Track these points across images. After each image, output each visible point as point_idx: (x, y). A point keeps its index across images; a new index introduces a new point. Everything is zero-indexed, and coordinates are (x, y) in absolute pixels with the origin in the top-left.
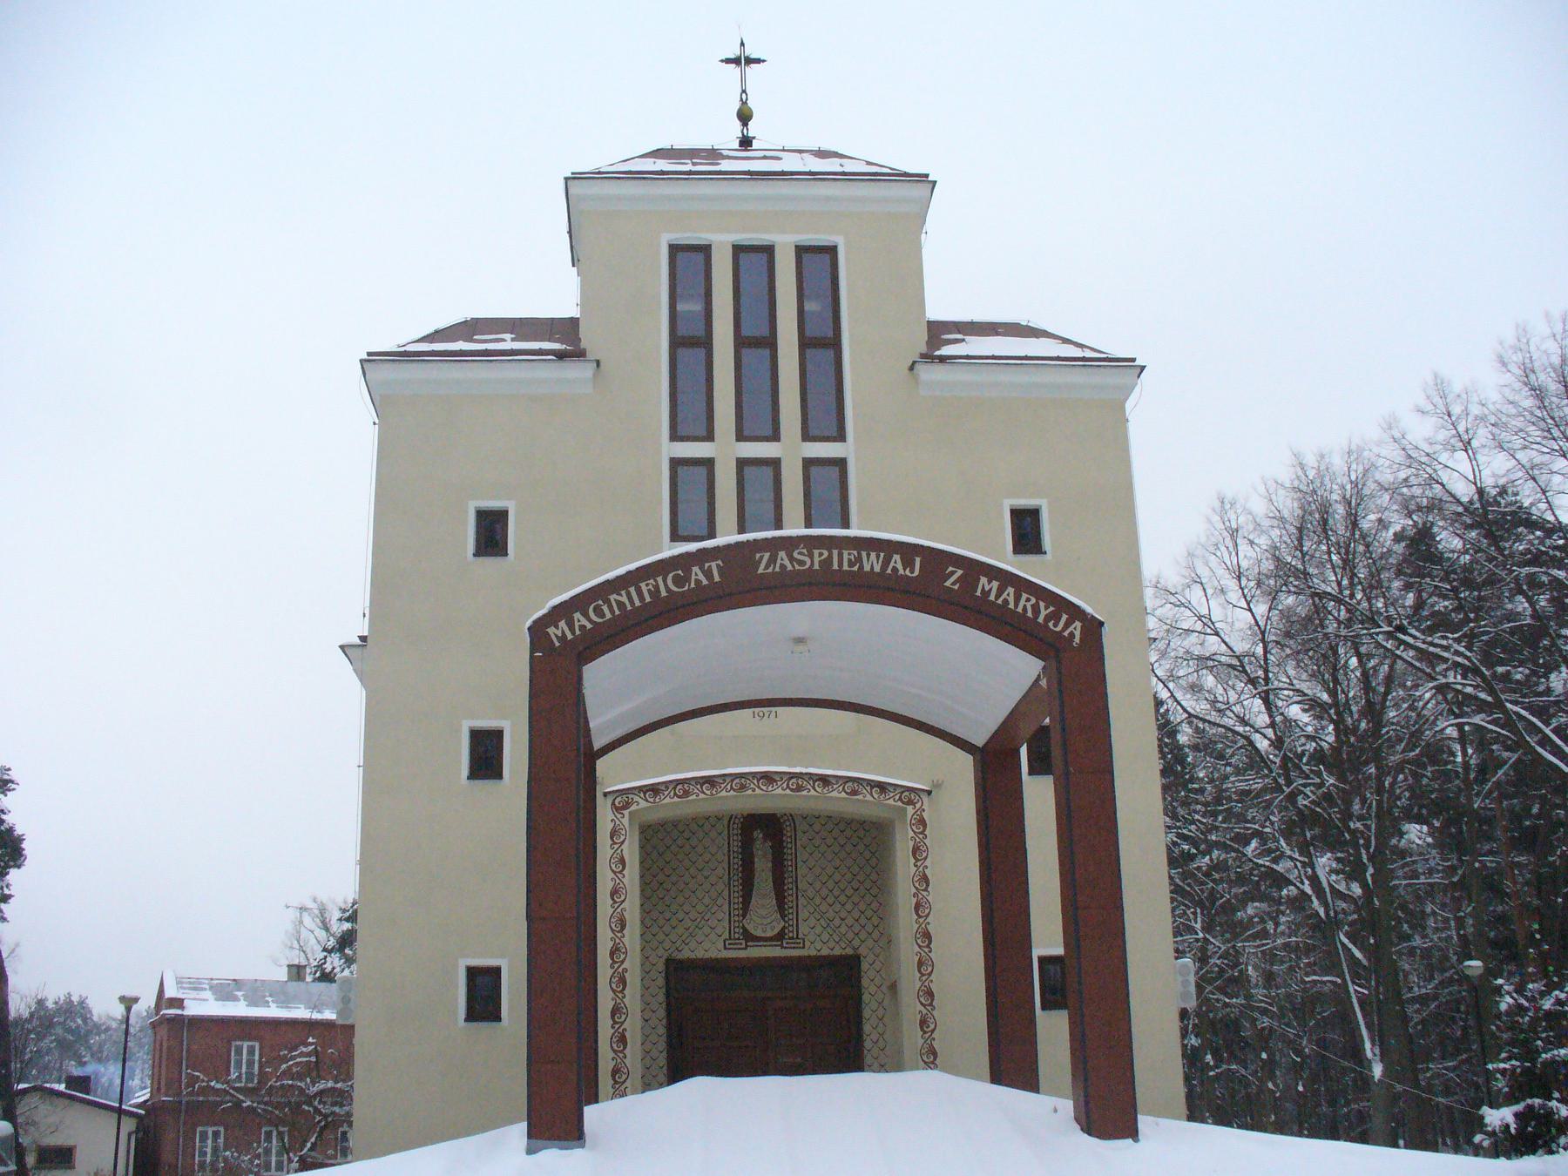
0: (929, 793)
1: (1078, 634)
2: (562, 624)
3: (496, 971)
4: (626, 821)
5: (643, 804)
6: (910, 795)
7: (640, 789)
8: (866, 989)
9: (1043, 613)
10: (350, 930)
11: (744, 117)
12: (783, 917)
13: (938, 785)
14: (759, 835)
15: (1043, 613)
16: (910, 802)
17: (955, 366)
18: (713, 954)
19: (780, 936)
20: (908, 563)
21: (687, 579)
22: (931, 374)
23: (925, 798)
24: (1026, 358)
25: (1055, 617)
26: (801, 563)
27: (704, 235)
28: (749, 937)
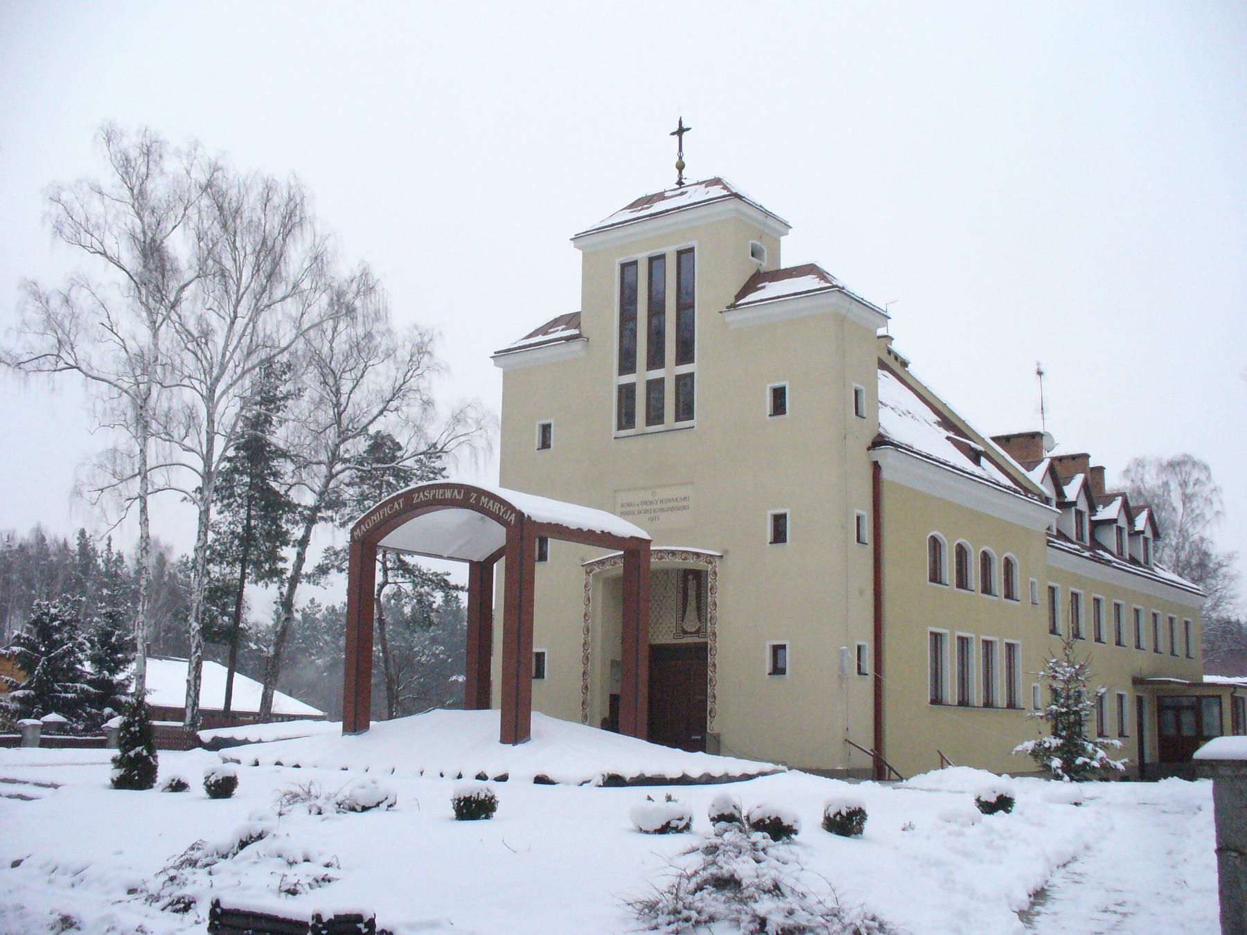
0: (721, 557)
1: (513, 520)
2: (358, 530)
3: (544, 653)
4: (591, 579)
5: (598, 570)
6: (710, 559)
7: (597, 562)
8: (382, 672)
9: (502, 510)
10: (92, 662)
11: (680, 167)
12: (700, 620)
13: (726, 552)
14: (690, 577)
15: (502, 510)
16: (711, 563)
17: (739, 311)
18: (668, 642)
19: (698, 632)
20: (459, 493)
21: (393, 507)
22: (733, 316)
23: (717, 560)
24: (778, 297)
25: (505, 512)
26: (427, 497)
27: (633, 256)
28: (685, 632)
